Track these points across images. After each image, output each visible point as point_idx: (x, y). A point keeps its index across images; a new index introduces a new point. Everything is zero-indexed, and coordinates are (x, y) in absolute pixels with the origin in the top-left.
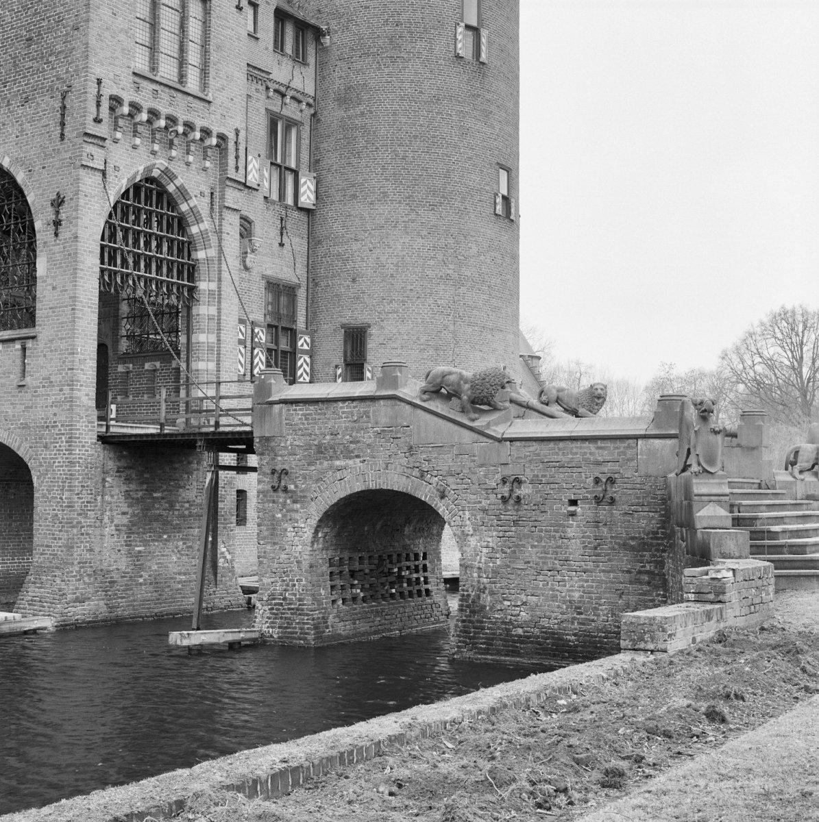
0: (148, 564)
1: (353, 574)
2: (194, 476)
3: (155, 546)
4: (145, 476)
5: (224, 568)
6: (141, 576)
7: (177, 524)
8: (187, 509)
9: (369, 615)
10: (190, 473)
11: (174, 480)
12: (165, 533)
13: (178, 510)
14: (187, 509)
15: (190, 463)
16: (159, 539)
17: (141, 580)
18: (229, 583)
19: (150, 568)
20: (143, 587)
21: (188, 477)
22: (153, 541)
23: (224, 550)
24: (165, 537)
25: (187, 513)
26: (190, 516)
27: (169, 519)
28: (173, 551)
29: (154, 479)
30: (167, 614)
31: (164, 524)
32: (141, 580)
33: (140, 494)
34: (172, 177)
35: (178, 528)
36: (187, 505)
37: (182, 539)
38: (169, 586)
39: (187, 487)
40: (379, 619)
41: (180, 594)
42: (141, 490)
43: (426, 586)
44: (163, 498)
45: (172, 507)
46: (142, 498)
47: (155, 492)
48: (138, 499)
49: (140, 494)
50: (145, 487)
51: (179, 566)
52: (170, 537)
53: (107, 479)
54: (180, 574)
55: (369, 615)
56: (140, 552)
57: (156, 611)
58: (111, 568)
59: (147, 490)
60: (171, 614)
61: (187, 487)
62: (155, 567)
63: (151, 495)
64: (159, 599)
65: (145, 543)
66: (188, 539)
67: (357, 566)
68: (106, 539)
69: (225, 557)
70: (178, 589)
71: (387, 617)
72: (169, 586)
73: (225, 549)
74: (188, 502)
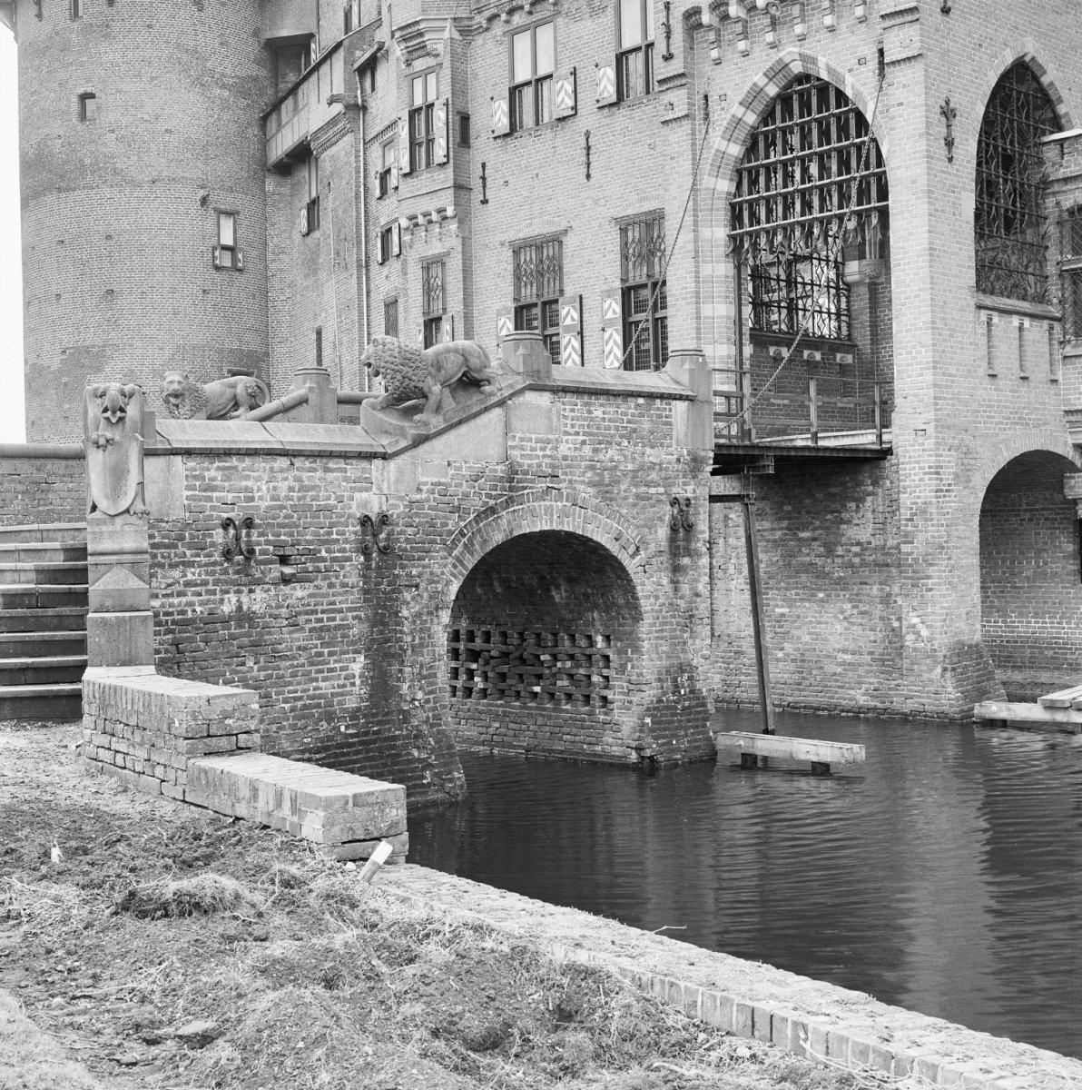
0: (797, 633)
1: (474, 655)
2: (867, 504)
3: (808, 610)
4: (785, 508)
5: (915, 650)
6: (782, 649)
7: (840, 578)
8: (856, 555)
9: (483, 716)
10: (860, 500)
11: (832, 512)
12: (820, 590)
13: (842, 556)
14: (856, 555)
15: (859, 484)
16: (811, 598)
17: (780, 654)
18: (926, 676)
19: (799, 638)
20: (780, 664)
21: (858, 506)
22: (802, 600)
23: (915, 620)
24: (821, 595)
25: (857, 560)
26: (862, 565)
27: (827, 569)
28: (836, 617)
29: (799, 513)
30: (805, 707)
31: (817, 577)
32: (780, 654)
33: (779, 534)
34: (757, 92)
35: (841, 584)
36: (856, 549)
37: (850, 601)
38: (821, 668)
39: (855, 521)
40: (497, 725)
41: (837, 681)
42: (781, 529)
43: (605, 692)
44: (814, 539)
45: (830, 551)
46: (781, 540)
47: (803, 530)
48: (775, 541)
49: (779, 534)
50: (785, 524)
51: (846, 640)
52: (829, 595)
53: (731, 516)
54: (845, 651)
55: (483, 716)
56: (783, 615)
57: (790, 699)
58: (742, 634)
59: (788, 529)
60: (811, 708)
61: (855, 521)
62: (806, 638)
63: (796, 534)
64: (800, 684)
65: (790, 603)
66: (860, 601)
67: (478, 643)
68: (733, 595)
69: (918, 634)
70: (835, 674)
71: (511, 726)
72: (821, 668)
73: (918, 620)
74: (858, 544)
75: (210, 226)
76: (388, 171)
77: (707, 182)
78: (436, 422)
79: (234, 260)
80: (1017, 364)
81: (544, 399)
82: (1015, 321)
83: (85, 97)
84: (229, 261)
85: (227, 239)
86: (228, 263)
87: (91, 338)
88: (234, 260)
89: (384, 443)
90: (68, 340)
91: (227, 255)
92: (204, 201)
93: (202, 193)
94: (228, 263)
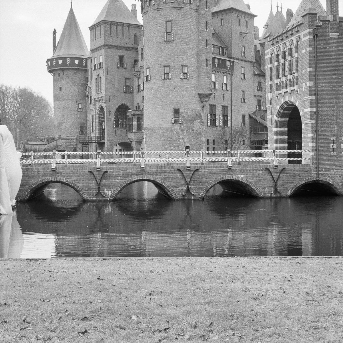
75: (77, 105)
76: (148, 76)
77: (96, 115)
78: (50, 142)
79: (81, 110)
80: (120, 133)
81: (60, 140)
82: (120, 130)
83: (60, 88)
84: (80, 110)
85: (80, 107)
86: (80, 110)
87: (61, 121)
88: (81, 110)
89: (46, 144)
90: (58, 122)
91: (80, 109)
92: (76, 102)
93: (76, 101)
94: (80, 110)
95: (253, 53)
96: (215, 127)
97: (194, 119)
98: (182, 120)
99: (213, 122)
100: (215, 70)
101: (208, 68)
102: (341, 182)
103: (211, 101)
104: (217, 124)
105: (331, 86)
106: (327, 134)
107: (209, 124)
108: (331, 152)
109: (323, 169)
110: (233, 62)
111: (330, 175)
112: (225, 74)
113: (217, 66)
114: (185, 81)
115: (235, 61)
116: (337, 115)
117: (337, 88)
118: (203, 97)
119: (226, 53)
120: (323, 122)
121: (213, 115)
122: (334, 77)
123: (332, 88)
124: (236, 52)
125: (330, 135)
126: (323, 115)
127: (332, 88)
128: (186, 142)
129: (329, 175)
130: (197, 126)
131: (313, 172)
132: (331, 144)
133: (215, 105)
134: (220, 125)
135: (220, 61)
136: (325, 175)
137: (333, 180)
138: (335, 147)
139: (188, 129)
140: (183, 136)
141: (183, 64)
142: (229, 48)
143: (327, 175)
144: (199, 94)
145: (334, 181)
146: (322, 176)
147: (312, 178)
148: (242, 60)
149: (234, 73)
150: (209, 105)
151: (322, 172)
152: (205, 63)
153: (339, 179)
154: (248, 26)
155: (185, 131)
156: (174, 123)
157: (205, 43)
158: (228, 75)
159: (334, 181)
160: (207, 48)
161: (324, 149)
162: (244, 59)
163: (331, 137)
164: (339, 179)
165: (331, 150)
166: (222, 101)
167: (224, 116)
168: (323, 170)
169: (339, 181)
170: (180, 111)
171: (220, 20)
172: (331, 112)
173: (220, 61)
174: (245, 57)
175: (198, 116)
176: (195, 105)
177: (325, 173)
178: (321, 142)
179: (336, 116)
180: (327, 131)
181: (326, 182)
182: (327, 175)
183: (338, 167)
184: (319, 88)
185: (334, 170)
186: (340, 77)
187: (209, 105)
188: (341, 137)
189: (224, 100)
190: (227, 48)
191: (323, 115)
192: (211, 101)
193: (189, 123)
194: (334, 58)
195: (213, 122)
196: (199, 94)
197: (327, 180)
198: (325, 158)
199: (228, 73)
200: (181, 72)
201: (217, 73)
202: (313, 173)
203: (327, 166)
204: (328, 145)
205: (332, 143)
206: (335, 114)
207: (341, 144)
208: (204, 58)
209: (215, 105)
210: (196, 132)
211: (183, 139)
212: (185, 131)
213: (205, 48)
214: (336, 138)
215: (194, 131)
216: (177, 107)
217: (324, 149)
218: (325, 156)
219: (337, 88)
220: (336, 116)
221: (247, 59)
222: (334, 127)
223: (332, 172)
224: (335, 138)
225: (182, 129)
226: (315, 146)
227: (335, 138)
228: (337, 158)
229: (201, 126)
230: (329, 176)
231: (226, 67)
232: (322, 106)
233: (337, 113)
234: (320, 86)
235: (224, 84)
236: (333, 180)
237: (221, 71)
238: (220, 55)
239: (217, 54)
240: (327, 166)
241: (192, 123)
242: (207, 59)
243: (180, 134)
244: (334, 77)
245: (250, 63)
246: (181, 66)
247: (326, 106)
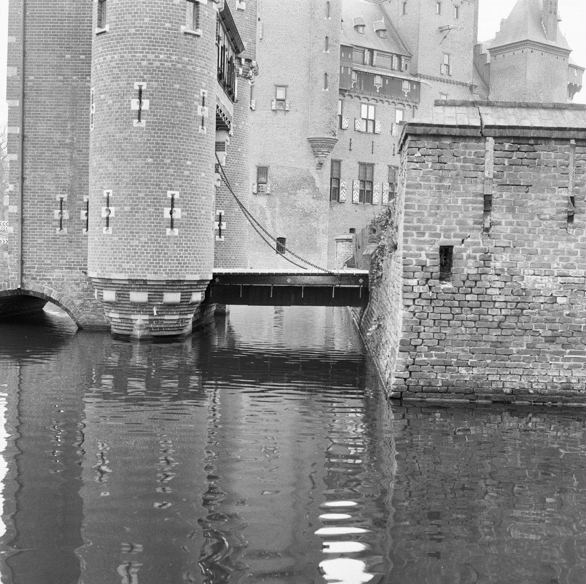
95: (469, 66)
96: (371, 206)
97: (297, 187)
98: (272, 187)
99: (335, 194)
100: (376, 98)
101: (327, 90)
102: (79, 298)
103: (333, 155)
104: (376, 200)
105: (60, 78)
106: (47, 187)
107: (356, 198)
108: (57, 227)
109: (36, 266)
110: (418, 83)
111: (53, 280)
112: (400, 106)
113: (378, 91)
114: (280, 115)
115: (422, 81)
116: (72, 144)
117: (73, 81)
118: (318, 146)
119: (408, 66)
120: (38, 159)
121: (336, 179)
122: (68, 56)
123: (60, 81)
124: (426, 64)
125: (53, 188)
126: (37, 144)
127: (60, 81)
128: (278, 230)
129: (49, 279)
130: (304, 199)
131: (12, 271)
132: (56, 209)
133: (372, 165)
134: (382, 203)
135: (387, 81)
136: (40, 279)
137: (60, 291)
138: (66, 216)
139: (283, 205)
140: (273, 217)
141: (278, 83)
142: (413, 57)
143: (46, 279)
144: (311, 141)
145: (63, 295)
146: (33, 281)
147: (9, 285)
148: (441, 80)
149: (419, 106)
150: (359, 163)
151: (33, 272)
152: (321, 82)
153: (75, 291)
154: (460, 15)
155: (277, 209)
156: (256, 192)
157: (324, 44)
158: (407, 108)
159: (63, 295)
160: (328, 52)
161: (38, 220)
162: (447, 77)
163: (56, 193)
164: (75, 291)
165: (57, 223)
166: (347, 151)
167: (363, 182)
168: (34, 268)
169: (74, 294)
170: (269, 172)
171: (403, 4)
172: (58, 136)
173: (387, 81)
174: (449, 74)
175: (308, 181)
176: (304, 162)
177: (39, 276)
178: (31, 205)
179: (71, 146)
180: (47, 180)
181: (43, 294)
182: (46, 279)
183: (73, 262)
184: (31, 81)
185: (62, 268)
186: (83, 57)
187: (359, 163)
188: (81, 193)
189: (350, 150)
190: (410, 57)
191: (37, 144)
192: (333, 155)
193: (286, 194)
194: (68, 14)
195: (335, 194)
196: (311, 141)
197: (45, 292)
198: (39, 241)
199: (406, 103)
200: (274, 97)
201: (380, 103)
202: (12, 274)
203: (45, 258)
204: (49, 211)
205: (59, 207)
206: (67, 141)
207: (80, 209)
208: (320, 72)
209: (372, 165)
210: (301, 210)
211: (273, 224)
212: (277, 209)
213: (324, 52)
214: (68, 196)
215: (296, 210)
216: (263, 164)
217: (38, 220)
218: (41, 235)
219: (73, 81)
220: (71, 146)
221: (453, 78)
222: (65, 172)
223: (57, 274)
224: (65, 197)
225: (271, 206)
226: (17, 214)
227: (65, 197)
228: (71, 242)
229: (312, 201)
230: (49, 283)
231: (400, 92)
232: (36, 123)
233: (72, 139)
234: (32, 78)
235: (395, 124)
236: (60, 291)
237: (390, 100)
238: (392, 69)
239: (386, 68)
240: (45, 258)
241: (291, 194)
242: (326, 74)
243: (268, 214)
244: (68, 56)
245: (461, 86)
246: (274, 87)
247: (47, 123)
